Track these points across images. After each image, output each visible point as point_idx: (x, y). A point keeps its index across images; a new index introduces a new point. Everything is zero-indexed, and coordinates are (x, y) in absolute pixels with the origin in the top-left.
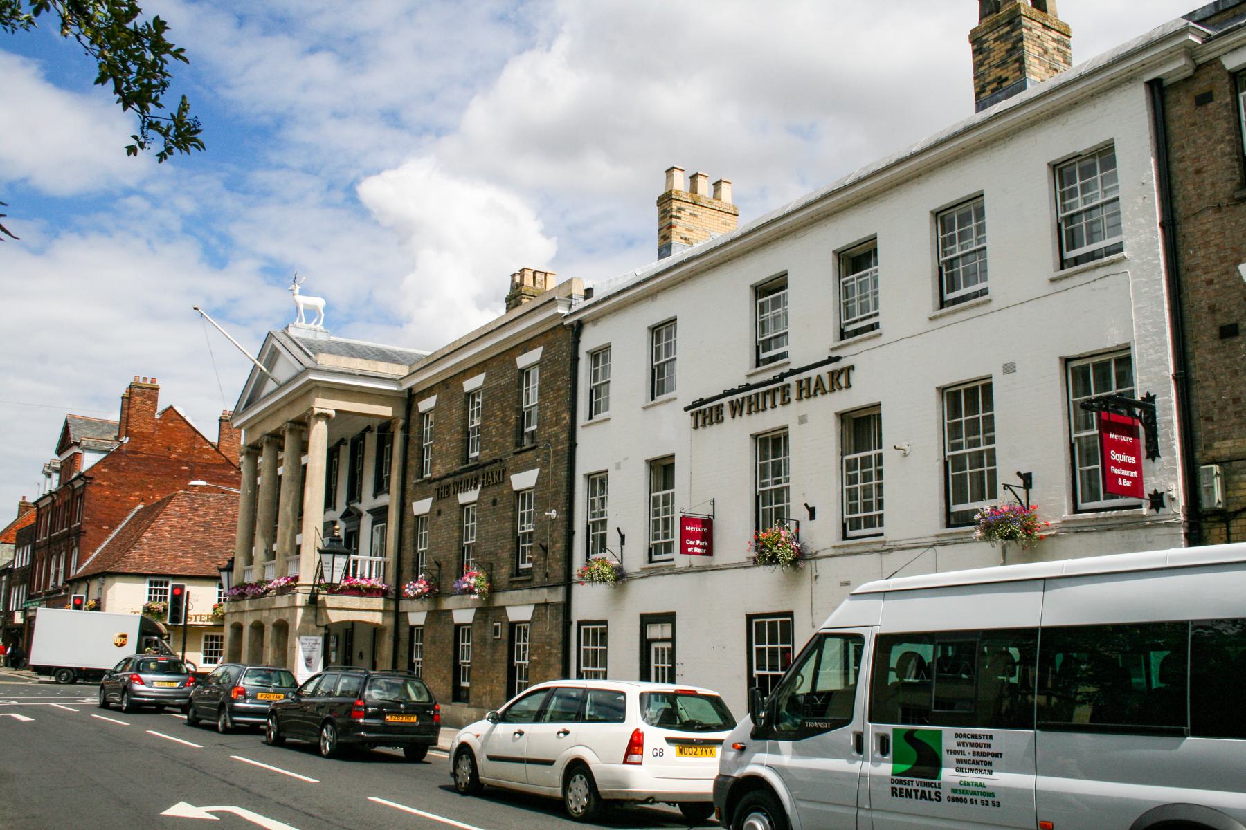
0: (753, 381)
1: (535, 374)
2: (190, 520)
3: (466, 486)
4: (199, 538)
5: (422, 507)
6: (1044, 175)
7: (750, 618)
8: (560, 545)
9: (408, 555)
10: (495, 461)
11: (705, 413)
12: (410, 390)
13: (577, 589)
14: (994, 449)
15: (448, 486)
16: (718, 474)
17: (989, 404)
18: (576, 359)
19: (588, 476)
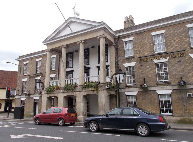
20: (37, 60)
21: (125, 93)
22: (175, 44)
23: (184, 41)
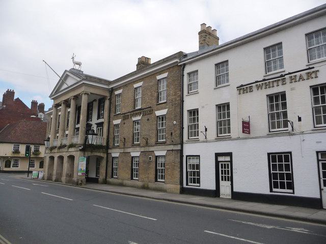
0: (266, 78)
1: (140, 91)
3: (136, 115)
5: (117, 122)
6: (262, 51)
7: (269, 154)
8: (178, 132)
9: (111, 136)
11: (243, 89)
13: (185, 146)
15: (128, 116)
16: (255, 108)
17: (228, 109)
18: (183, 76)
19: (188, 111)
20: (136, 86)
21: (155, 152)
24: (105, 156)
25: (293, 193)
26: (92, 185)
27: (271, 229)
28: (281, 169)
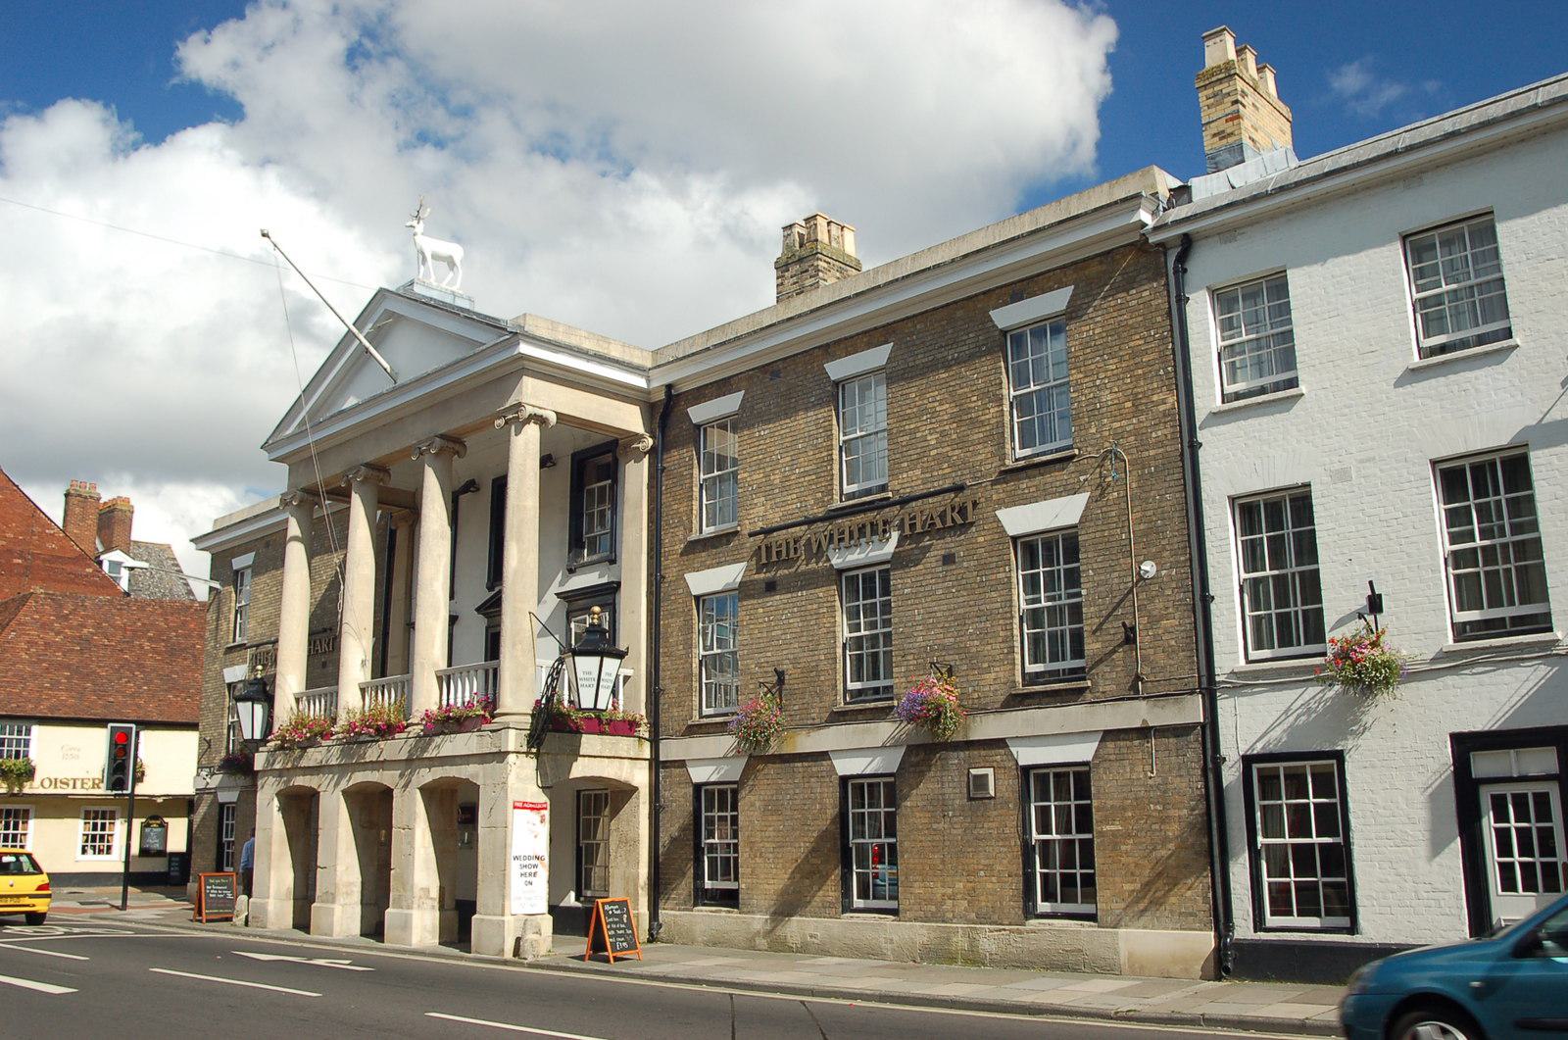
2: (58, 634)
4: (74, 660)
10: (325, 630)
12: (669, 387)
13: (1224, 705)
14: (29, 740)
22: (932, 440)
23: (975, 423)
24: (639, 776)
25: (1353, 929)
26: (1431, 988)
27: (72, 993)
28: (1300, 827)
